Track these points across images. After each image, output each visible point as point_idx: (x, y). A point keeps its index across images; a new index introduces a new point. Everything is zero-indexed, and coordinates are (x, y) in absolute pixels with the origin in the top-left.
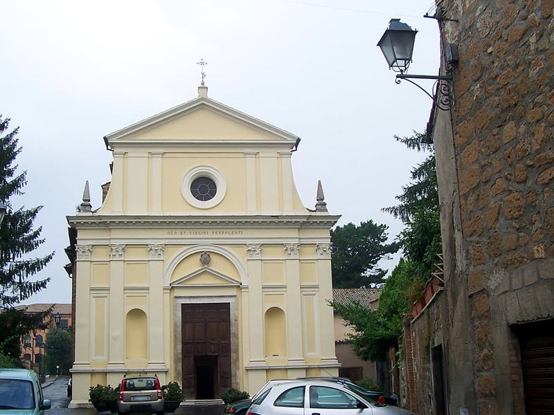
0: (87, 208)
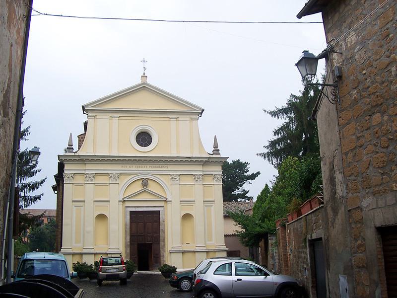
0: (71, 150)
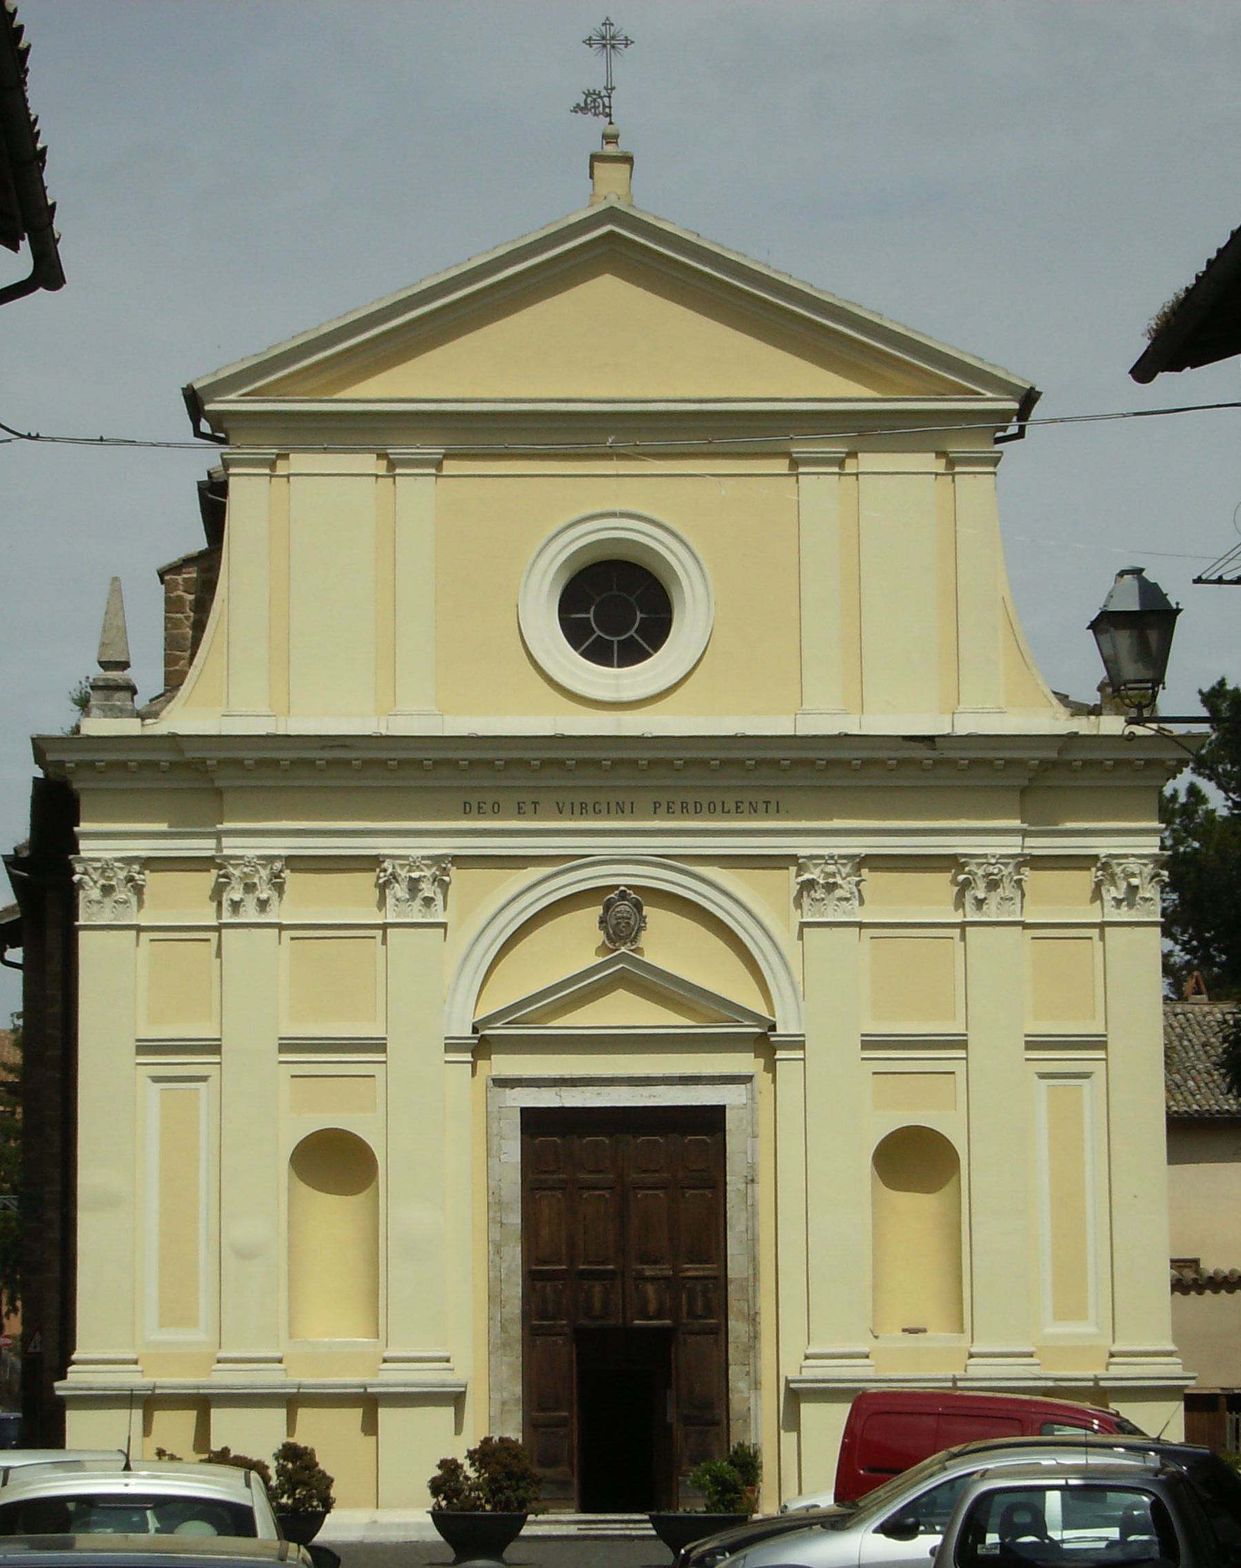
0: (119, 699)
